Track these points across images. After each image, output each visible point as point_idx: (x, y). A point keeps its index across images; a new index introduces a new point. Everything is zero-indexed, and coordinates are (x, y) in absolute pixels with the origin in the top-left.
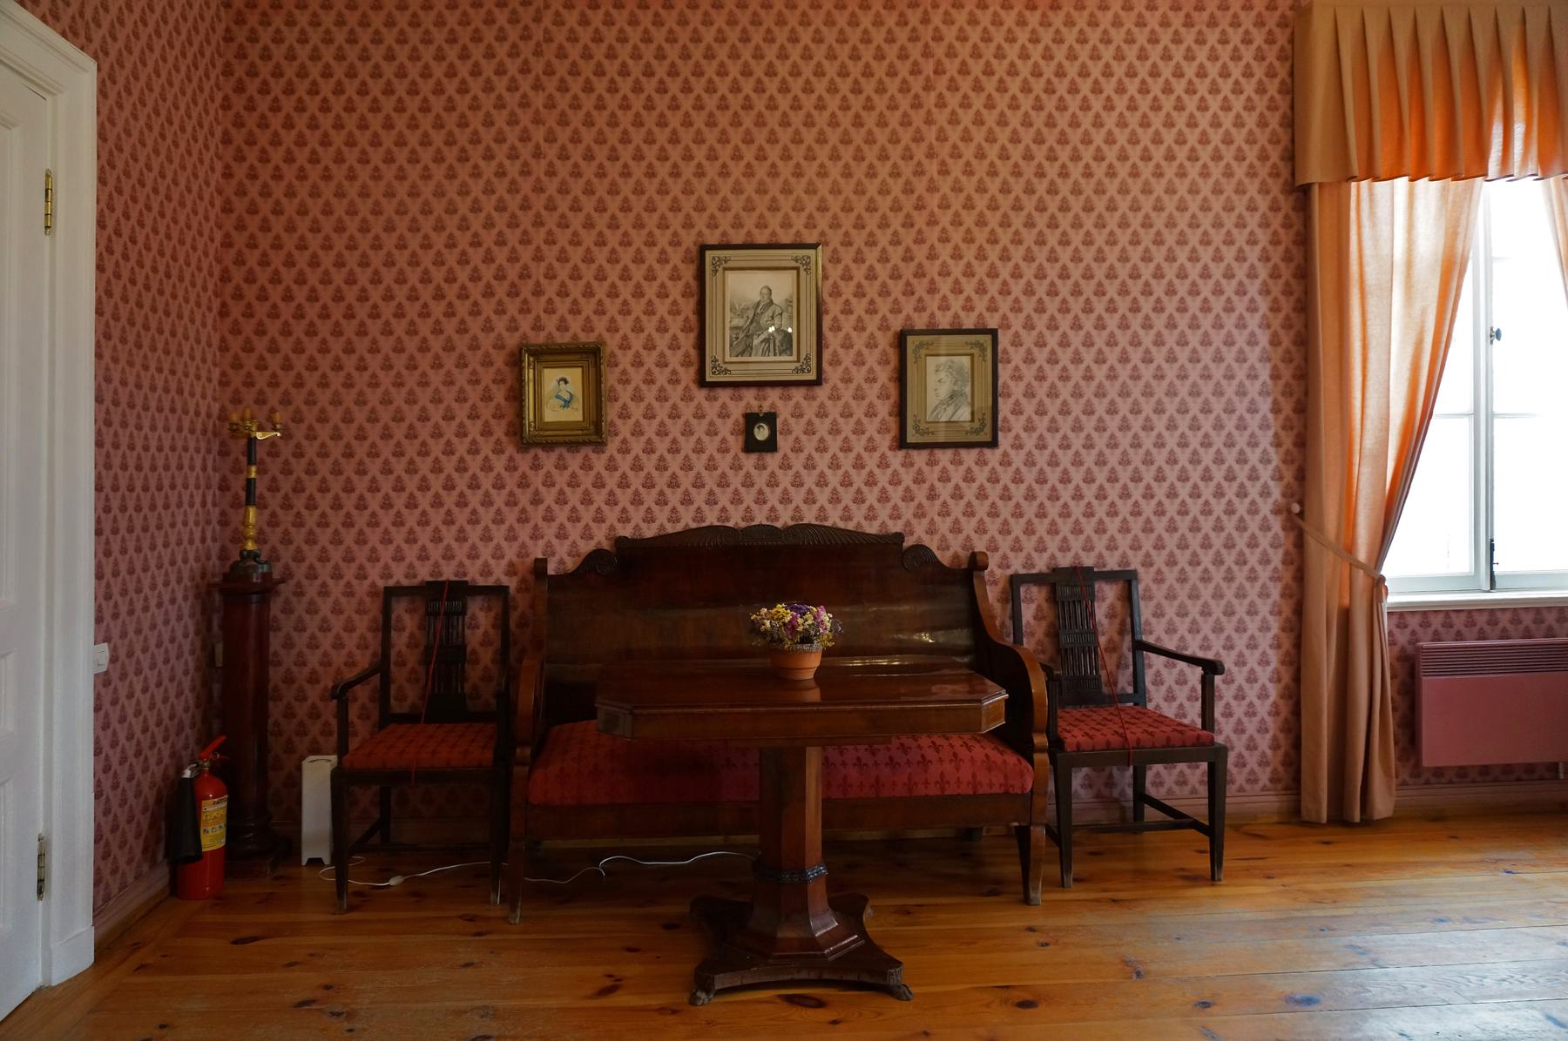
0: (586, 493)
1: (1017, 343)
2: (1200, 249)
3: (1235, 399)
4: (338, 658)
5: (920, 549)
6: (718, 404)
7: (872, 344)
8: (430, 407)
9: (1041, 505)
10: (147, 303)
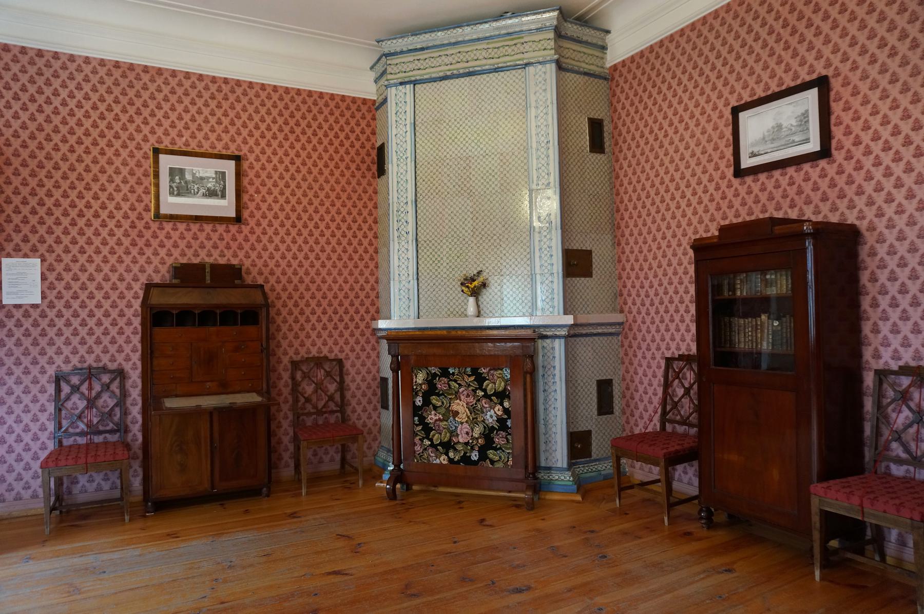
1: (353, 365)
2: (356, 113)
5: (722, 229)
9: (335, 324)
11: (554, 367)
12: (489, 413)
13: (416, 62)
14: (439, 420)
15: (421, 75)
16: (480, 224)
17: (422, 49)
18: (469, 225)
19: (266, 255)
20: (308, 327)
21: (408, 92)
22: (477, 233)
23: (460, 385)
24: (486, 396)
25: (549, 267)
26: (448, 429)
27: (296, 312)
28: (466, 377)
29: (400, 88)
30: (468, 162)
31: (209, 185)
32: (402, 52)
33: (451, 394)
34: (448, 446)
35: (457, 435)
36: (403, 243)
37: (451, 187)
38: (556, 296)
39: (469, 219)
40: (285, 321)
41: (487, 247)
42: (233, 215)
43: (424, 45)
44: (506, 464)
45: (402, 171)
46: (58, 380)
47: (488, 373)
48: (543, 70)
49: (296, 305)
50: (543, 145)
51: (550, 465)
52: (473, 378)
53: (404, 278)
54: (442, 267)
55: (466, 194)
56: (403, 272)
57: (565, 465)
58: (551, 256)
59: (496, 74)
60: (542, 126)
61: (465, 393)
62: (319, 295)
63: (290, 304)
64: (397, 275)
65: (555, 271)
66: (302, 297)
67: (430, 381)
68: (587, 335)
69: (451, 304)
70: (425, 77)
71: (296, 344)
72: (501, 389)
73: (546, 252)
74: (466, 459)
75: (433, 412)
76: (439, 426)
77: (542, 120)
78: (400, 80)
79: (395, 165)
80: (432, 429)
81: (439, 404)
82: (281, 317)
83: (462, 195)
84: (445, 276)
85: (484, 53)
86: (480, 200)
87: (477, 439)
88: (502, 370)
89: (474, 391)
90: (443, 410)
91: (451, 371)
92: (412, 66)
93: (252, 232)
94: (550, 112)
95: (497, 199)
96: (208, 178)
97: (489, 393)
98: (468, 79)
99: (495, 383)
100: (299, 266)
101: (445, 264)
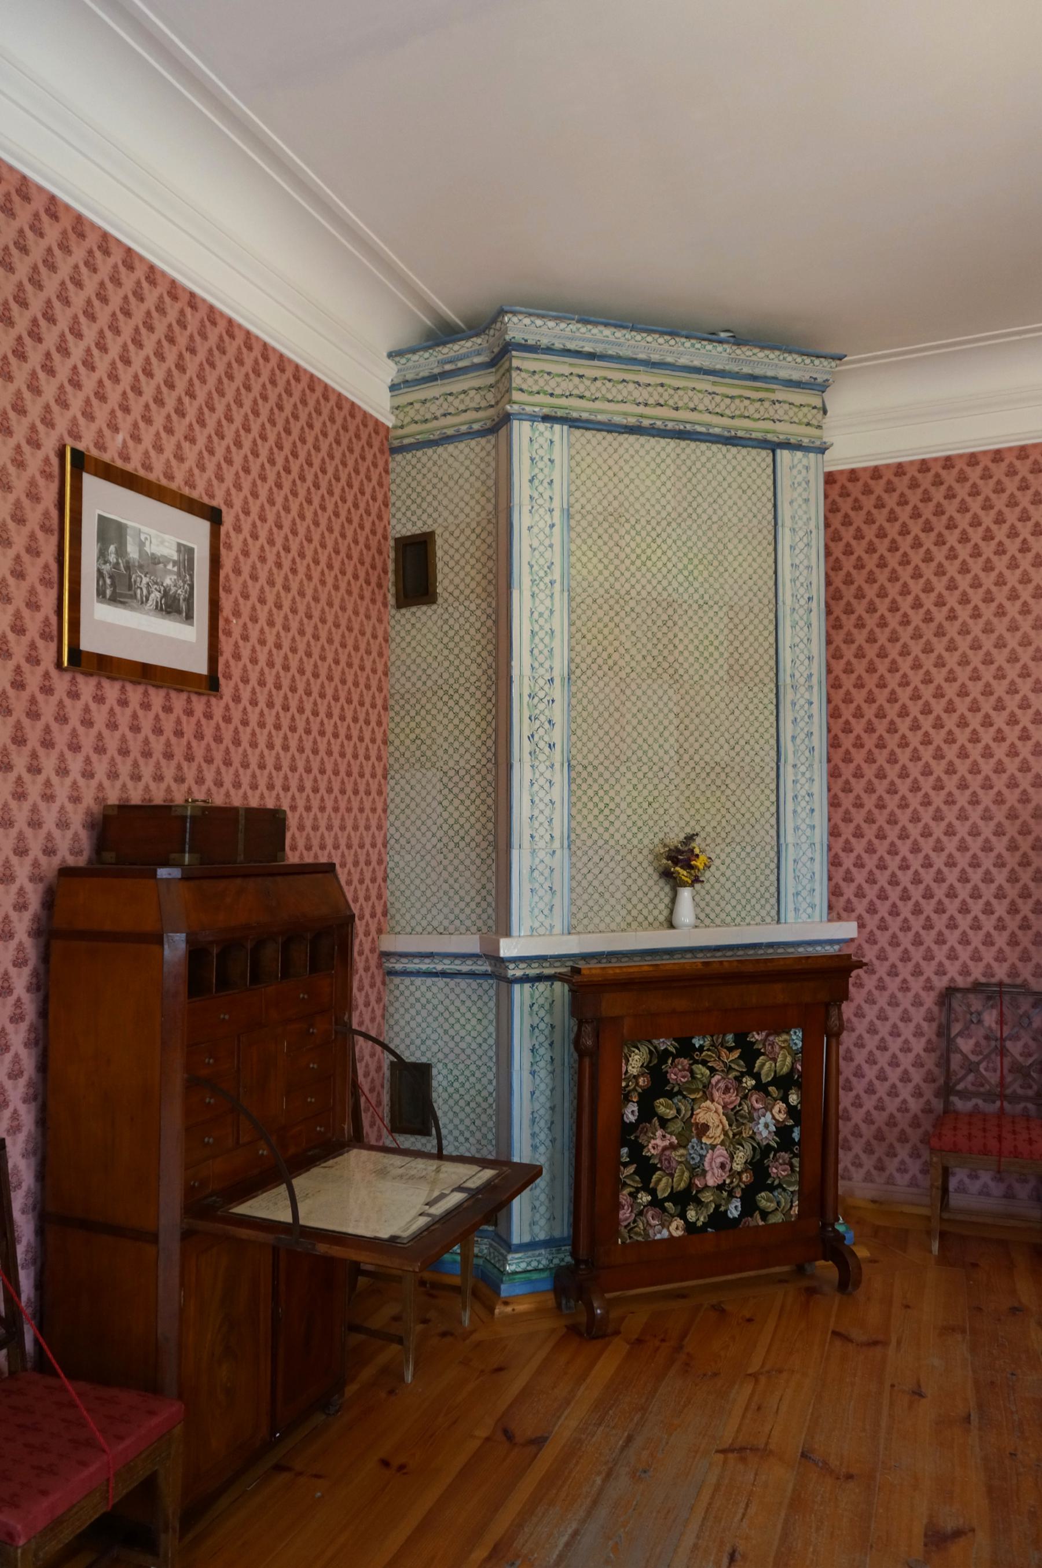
0: (871, 662)
4: (892, 1105)
7: (917, 1003)
10: (323, 635)
12: (762, 1120)
13: (576, 380)
14: (672, 1147)
15: (591, 412)
16: (692, 739)
17: (592, 356)
18: (672, 740)
21: (556, 438)
22: (686, 757)
23: (713, 1070)
24: (761, 1087)
25: (808, 832)
26: (686, 1163)
28: (724, 1053)
29: (541, 426)
30: (670, 611)
31: (168, 581)
32: (549, 350)
33: (697, 1091)
34: (685, 1198)
35: (704, 1173)
36: (542, 768)
37: (639, 657)
39: (672, 728)
41: (703, 787)
42: (201, 667)
43: (599, 349)
44: (787, 1214)
45: (541, 608)
48: (805, 462)
50: (802, 602)
52: (736, 1054)
53: (542, 844)
54: (617, 824)
55: (666, 676)
56: (542, 831)
58: (812, 811)
59: (724, 449)
60: (802, 567)
61: (722, 1085)
64: (526, 838)
65: (817, 839)
67: (655, 1070)
69: (635, 900)
70: (600, 417)
72: (785, 1070)
73: (803, 804)
74: (718, 1219)
75: (659, 1133)
77: (802, 556)
78: (546, 411)
79: (527, 594)
80: (654, 1169)
81: (671, 1113)
83: (660, 676)
84: (623, 842)
85: (707, 400)
86: (692, 692)
87: (740, 1174)
88: (788, 1033)
89: (738, 1079)
90: (677, 1126)
91: (697, 1042)
92: (566, 386)
94: (814, 543)
95: (723, 694)
96: (166, 560)
97: (765, 1079)
98: (673, 443)
99: (775, 1060)
101: (623, 817)
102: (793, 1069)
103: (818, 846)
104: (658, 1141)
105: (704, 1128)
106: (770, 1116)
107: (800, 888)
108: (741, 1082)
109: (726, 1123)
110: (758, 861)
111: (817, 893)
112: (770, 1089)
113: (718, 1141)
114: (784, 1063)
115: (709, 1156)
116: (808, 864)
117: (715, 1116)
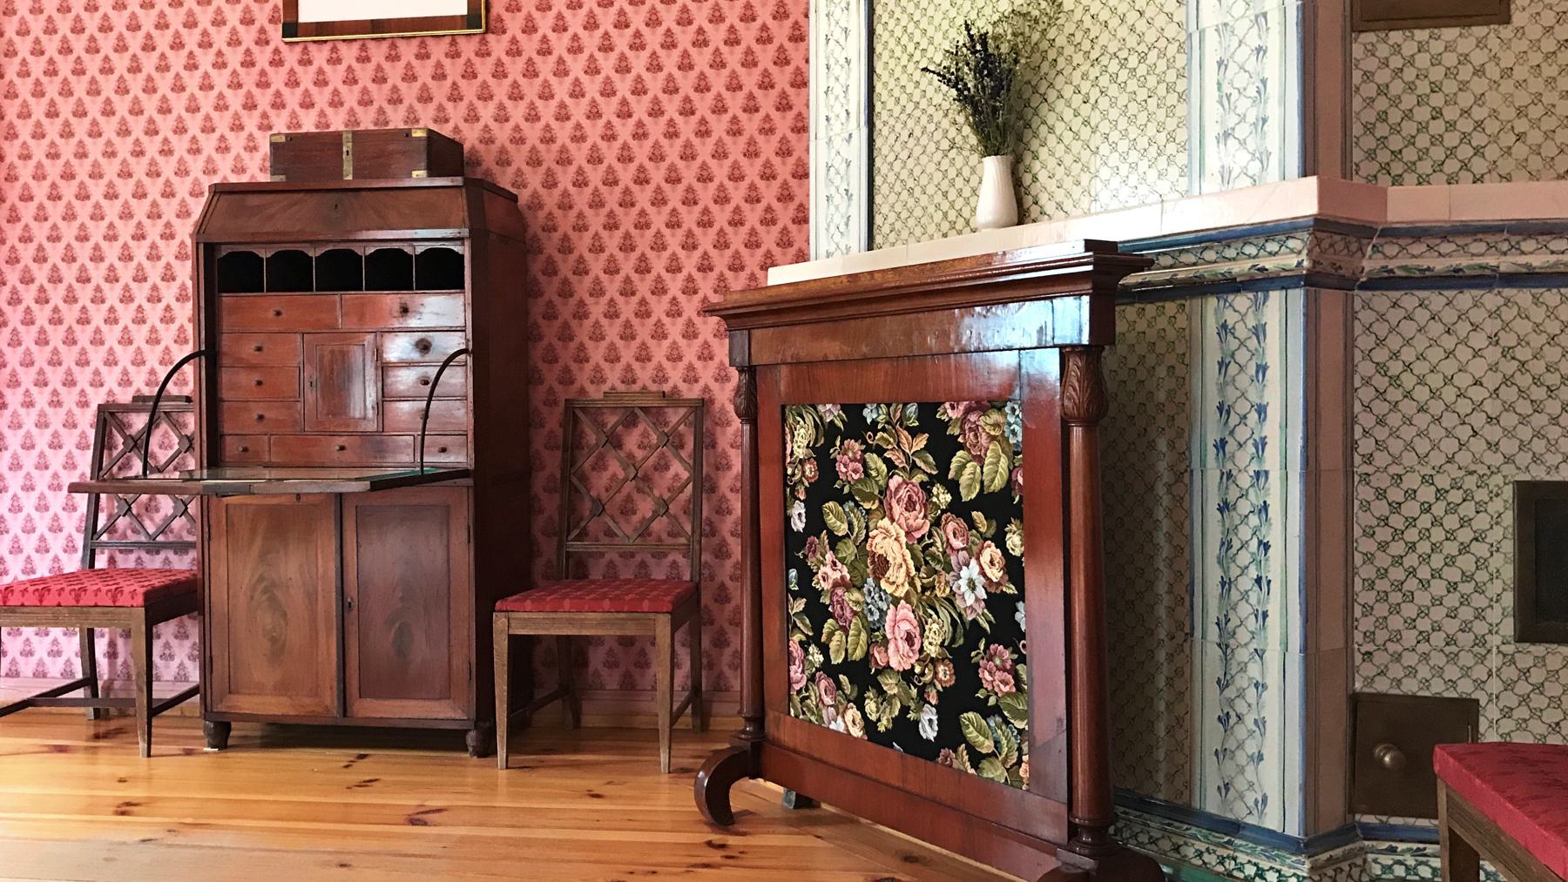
3: (682, 342)
6: (21, 639)
8: (713, 163)
11: (1261, 410)
12: (965, 573)
19: (547, 111)
20: (659, 307)
23: (890, 465)
24: (959, 508)
27: (627, 265)
33: (869, 497)
35: (885, 642)
38: (1273, 111)
40: (597, 291)
46: (109, 417)
47: (964, 420)
49: (627, 246)
51: (1239, 812)
52: (921, 442)
57: (1294, 829)
61: (903, 493)
62: (690, 217)
63: (612, 242)
66: (642, 225)
67: (822, 454)
68: (1456, 280)
71: (628, 354)
72: (998, 483)
74: (905, 728)
75: (829, 556)
76: (841, 603)
82: (588, 281)
89: (926, 487)
91: (869, 414)
93: (515, 52)
97: (968, 495)
99: (980, 460)
100: (635, 136)
102: (1010, 483)
103: (1274, 18)
104: (827, 569)
105: (882, 565)
106: (977, 569)
107: (1232, 120)
108: (929, 493)
109: (911, 563)
110: (1152, 81)
111: (1273, 128)
112: (977, 516)
113: (901, 593)
114: (996, 470)
115: (890, 613)
116: (1251, 65)
117: (896, 545)
